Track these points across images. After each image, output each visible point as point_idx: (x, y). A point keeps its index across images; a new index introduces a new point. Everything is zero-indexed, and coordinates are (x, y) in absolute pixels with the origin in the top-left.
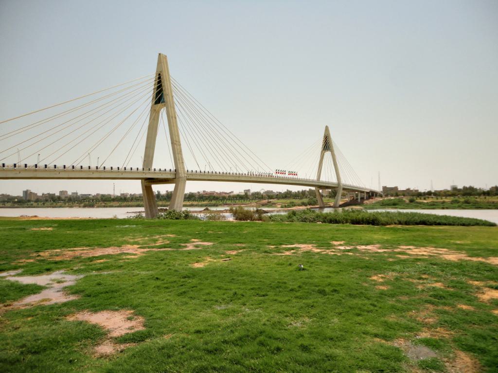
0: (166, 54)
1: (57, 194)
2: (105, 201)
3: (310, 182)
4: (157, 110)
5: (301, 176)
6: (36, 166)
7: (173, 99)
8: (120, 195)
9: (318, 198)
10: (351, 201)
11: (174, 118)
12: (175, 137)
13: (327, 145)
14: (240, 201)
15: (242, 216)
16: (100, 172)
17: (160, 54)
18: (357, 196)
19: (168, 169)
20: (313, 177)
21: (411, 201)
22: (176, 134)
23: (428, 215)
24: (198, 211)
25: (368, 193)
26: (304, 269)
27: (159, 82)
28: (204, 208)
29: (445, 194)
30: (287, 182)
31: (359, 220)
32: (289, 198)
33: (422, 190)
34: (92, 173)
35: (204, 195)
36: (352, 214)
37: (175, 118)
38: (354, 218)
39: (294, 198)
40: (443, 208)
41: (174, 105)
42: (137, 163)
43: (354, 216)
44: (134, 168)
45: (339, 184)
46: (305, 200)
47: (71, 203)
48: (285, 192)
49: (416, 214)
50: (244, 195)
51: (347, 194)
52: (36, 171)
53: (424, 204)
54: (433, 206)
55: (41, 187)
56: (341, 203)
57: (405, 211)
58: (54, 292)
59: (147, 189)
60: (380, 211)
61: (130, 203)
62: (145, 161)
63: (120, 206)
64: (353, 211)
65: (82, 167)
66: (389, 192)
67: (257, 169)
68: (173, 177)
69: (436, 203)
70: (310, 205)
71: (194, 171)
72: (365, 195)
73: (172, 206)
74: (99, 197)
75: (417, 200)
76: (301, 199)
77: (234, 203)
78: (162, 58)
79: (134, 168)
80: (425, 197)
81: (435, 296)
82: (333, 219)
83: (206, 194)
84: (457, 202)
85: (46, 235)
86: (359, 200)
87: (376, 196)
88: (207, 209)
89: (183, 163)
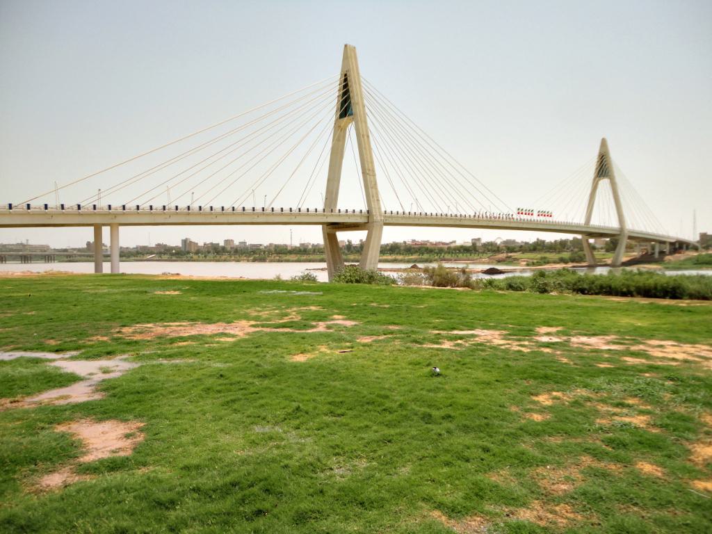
0: (354, 45)
1: (222, 244)
2: (280, 253)
3: (573, 226)
5: (559, 217)
6: (124, 207)
7: (364, 111)
8: (298, 245)
9: (586, 252)
10: (642, 256)
12: (368, 165)
13: (603, 169)
15: (444, 280)
16: (268, 215)
17: (346, 46)
18: (653, 248)
19: (357, 210)
20: (578, 219)
22: (369, 160)
26: (439, 375)
27: (346, 86)
30: (535, 227)
32: (540, 251)
34: (214, 217)
36: (637, 277)
37: (368, 137)
41: (365, 118)
42: (316, 202)
43: (642, 281)
44: (312, 209)
45: (622, 229)
46: (566, 255)
47: (237, 256)
48: (535, 242)
50: (470, 247)
51: (636, 246)
52: (189, 214)
55: (203, 235)
56: (624, 259)
58: (85, 386)
59: (330, 238)
61: (311, 257)
62: (326, 199)
64: (640, 273)
71: (394, 212)
72: (667, 249)
73: (363, 262)
74: (272, 249)
78: (349, 51)
79: (312, 209)
81: (610, 442)
82: (604, 285)
85: (171, 301)
86: (657, 255)
89: (378, 200)
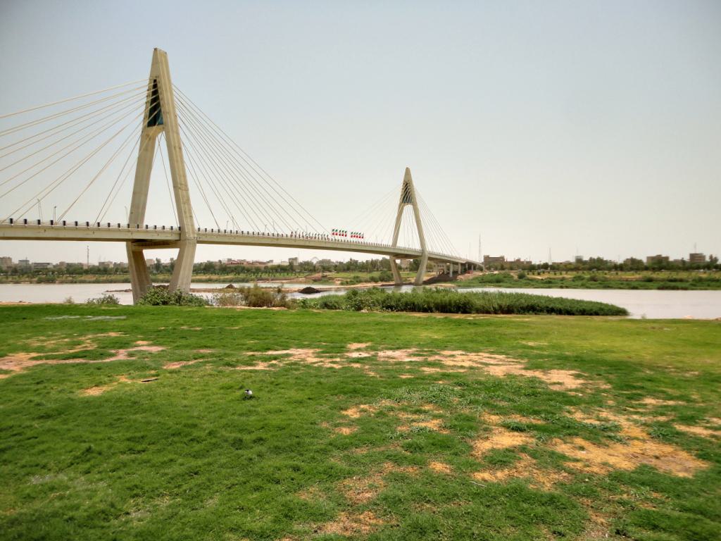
2: (73, 273)
4: (151, 135)
5: (370, 239)
7: (176, 121)
9: (394, 271)
10: (440, 275)
11: (178, 149)
13: (407, 196)
14: (282, 274)
17: (155, 49)
20: (387, 241)
21: (521, 277)
23: (538, 297)
24: (207, 291)
25: (462, 264)
26: (251, 397)
27: (155, 93)
28: (226, 285)
29: (566, 267)
31: (446, 304)
32: (353, 270)
33: (536, 261)
35: (228, 266)
36: (435, 295)
37: (180, 148)
38: (439, 301)
39: (360, 271)
40: (562, 287)
42: (119, 215)
43: (439, 298)
45: (423, 251)
46: (376, 274)
49: (522, 295)
53: (537, 281)
54: (549, 284)
56: (425, 278)
57: (508, 291)
59: (136, 257)
60: (475, 290)
61: (113, 277)
62: (131, 213)
63: (97, 282)
64: (438, 291)
65: (64, 222)
66: (492, 264)
67: (304, 228)
68: (177, 238)
69: (553, 281)
70: (382, 281)
72: (459, 268)
73: (174, 282)
74: (64, 268)
75: (528, 276)
76: (370, 272)
77: (273, 277)
80: (539, 271)
83: (232, 263)
84: (580, 278)
86: (451, 275)
87: (475, 269)
88: (230, 287)
89: (191, 217)
